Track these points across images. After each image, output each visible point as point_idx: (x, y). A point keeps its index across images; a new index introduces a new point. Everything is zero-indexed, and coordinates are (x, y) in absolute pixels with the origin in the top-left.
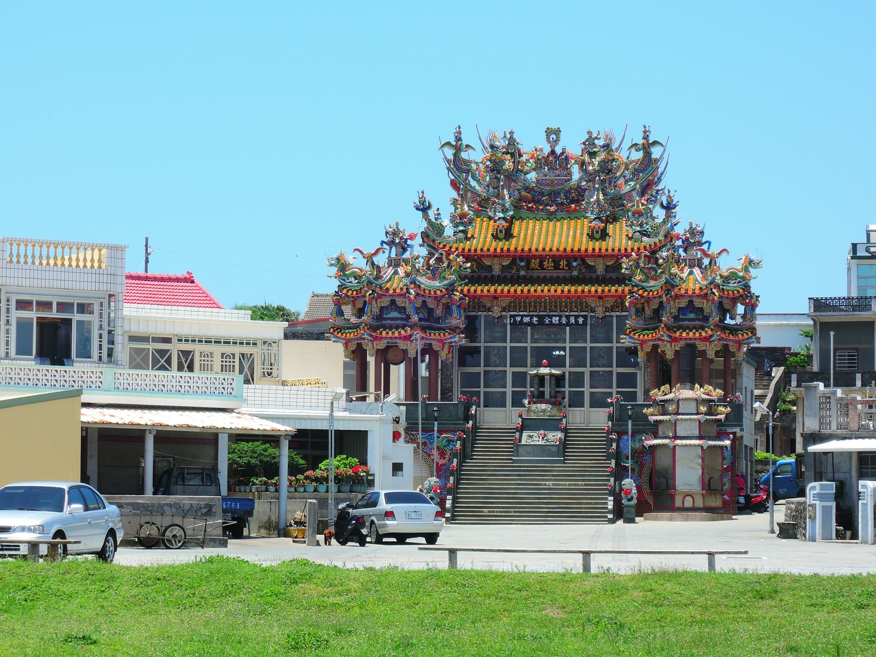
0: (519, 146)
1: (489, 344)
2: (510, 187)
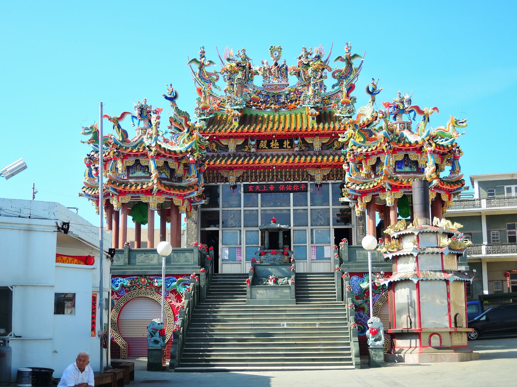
0: (250, 61)
1: (226, 209)
2: (242, 92)
